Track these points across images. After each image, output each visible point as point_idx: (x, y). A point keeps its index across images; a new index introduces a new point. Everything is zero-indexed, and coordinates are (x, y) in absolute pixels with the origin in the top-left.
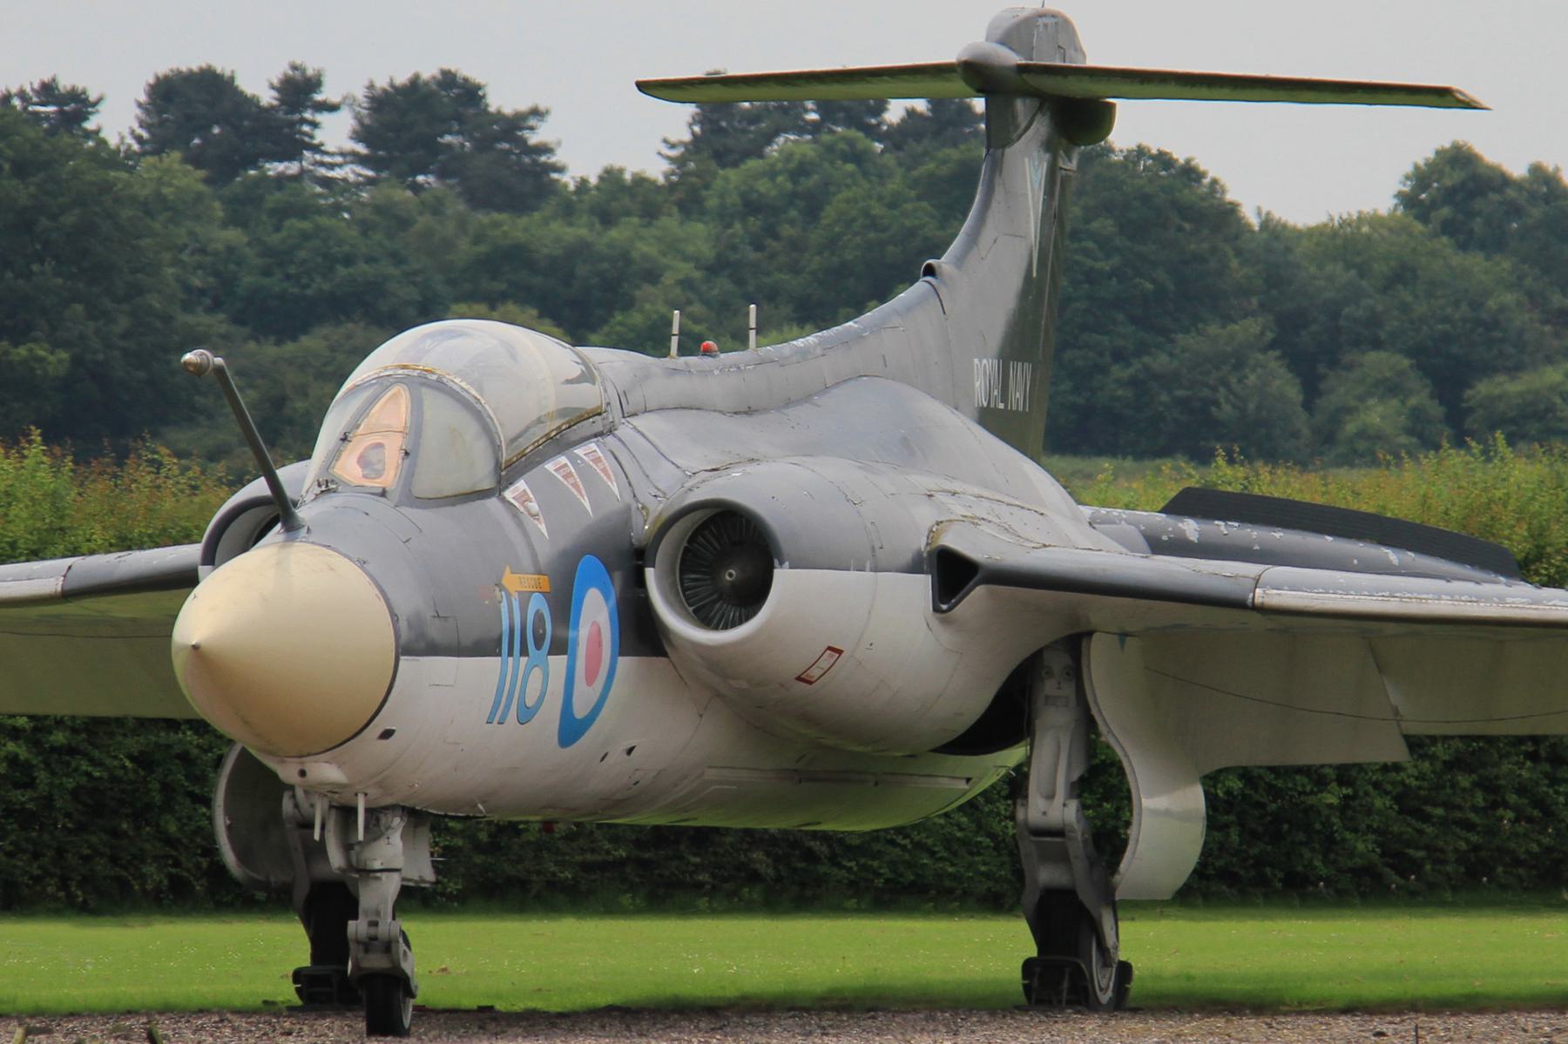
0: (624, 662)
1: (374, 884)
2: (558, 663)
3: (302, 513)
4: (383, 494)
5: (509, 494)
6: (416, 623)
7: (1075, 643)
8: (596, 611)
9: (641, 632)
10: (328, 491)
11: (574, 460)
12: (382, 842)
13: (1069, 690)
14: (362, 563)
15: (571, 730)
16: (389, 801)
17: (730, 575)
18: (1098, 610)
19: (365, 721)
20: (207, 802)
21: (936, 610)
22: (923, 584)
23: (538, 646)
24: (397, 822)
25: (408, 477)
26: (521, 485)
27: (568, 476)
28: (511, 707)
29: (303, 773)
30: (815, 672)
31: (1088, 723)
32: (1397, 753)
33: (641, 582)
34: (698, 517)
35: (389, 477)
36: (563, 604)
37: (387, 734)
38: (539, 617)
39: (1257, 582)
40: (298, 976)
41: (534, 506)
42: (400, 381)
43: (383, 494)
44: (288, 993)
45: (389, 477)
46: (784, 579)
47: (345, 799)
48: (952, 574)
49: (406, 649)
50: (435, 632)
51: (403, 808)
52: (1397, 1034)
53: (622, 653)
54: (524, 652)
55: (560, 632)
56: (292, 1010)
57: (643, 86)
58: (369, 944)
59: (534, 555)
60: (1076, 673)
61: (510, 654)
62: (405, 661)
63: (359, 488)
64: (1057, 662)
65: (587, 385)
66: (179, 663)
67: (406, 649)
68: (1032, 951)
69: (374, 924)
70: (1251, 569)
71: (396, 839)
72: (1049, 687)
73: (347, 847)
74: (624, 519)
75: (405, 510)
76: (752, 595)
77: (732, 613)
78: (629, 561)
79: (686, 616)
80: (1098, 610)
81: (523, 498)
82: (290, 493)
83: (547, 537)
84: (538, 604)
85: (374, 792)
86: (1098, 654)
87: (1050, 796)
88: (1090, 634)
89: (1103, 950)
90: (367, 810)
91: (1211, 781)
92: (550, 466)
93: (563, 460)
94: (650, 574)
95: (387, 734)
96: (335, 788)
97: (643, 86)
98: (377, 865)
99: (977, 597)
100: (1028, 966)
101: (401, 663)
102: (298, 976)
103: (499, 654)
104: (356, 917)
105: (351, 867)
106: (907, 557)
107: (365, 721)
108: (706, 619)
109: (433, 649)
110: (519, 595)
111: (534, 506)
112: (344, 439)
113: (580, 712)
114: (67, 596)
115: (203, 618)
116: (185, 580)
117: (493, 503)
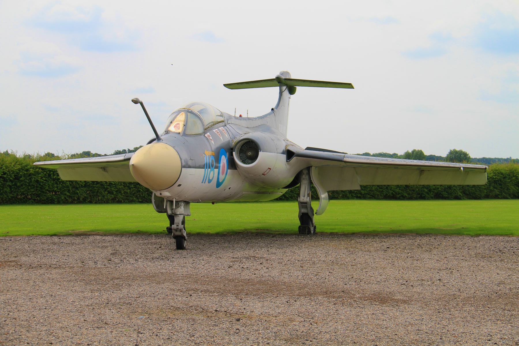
0: (229, 171)
1: (178, 217)
2: (216, 170)
5: (206, 135)
6: (186, 162)
7: (309, 168)
8: (224, 160)
9: (232, 165)
11: (219, 130)
12: (179, 208)
13: (307, 177)
14: (174, 147)
15: (219, 184)
16: (181, 200)
17: (250, 154)
18: (313, 162)
19: (175, 182)
20: (151, 196)
22: (284, 156)
23: (212, 167)
24: (182, 204)
26: (208, 134)
28: (207, 180)
29: (161, 194)
30: (266, 173)
31: (311, 183)
32: (359, 188)
33: (232, 155)
35: (180, 130)
36: (218, 159)
37: (180, 185)
39: (344, 157)
40: (167, 228)
41: (211, 138)
42: (183, 111)
43: (179, 133)
45: (180, 130)
46: (261, 154)
47: (171, 199)
48: (290, 154)
49: (183, 167)
50: (190, 163)
53: (229, 169)
54: (209, 168)
55: (217, 165)
57: (225, 85)
58: (176, 230)
59: (211, 148)
60: (309, 174)
62: (183, 169)
64: (305, 172)
66: (131, 168)
67: (183, 167)
68: (300, 225)
69: (178, 226)
71: (182, 207)
72: (304, 176)
73: (172, 209)
74: (229, 143)
75: (185, 138)
76: (254, 158)
77: (250, 161)
78: (231, 150)
80: (313, 162)
81: (209, 136)
83: (214, 144)
85: (177, 198)
87: (304, 196)
89: (312, 224)
90: (176, 202)
91: (328, 192)
94: (234, 153)
95: (180, 185)
96: (168, 197)
98: (178, 213)
99: (294, 159)
100: (299, 227)
105: (173, 213)
107: (175, 182)
108: (244, 162)
109: (190, 167)
110: (207, 157)
111: (211, 138)
112: (171, 123)
113: (220, 181)
117: (203, 136)
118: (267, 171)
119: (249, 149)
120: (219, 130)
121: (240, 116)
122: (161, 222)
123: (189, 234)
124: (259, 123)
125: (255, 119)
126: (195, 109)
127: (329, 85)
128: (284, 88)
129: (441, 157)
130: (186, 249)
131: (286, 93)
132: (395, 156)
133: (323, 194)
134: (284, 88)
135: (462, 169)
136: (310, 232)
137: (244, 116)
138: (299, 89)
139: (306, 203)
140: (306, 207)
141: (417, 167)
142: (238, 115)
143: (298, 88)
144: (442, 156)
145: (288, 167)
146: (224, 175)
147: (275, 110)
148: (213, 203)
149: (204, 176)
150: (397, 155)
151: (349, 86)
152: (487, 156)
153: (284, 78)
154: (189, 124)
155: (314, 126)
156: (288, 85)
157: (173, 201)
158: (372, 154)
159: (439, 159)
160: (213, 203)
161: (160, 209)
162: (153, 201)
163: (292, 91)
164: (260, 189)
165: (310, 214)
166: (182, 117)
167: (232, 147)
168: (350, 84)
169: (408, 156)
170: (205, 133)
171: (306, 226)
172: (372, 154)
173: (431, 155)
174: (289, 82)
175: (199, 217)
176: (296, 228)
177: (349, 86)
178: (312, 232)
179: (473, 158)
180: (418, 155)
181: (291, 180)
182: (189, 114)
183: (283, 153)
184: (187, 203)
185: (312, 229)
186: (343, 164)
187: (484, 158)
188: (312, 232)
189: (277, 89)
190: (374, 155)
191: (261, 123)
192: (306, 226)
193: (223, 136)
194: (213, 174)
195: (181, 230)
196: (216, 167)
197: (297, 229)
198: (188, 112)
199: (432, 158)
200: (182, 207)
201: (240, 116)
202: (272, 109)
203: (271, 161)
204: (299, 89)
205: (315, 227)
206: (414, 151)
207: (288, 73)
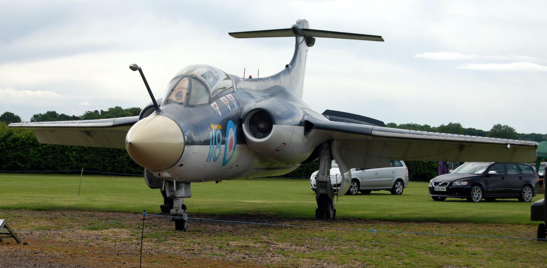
0: (237, 146)
3: (161, 108)
4: (182, 104)
6: (190, 137)
7: (329, 142)
8: (232, 134)
9: (241, 138)
10: (168, 103)
11: (226, 97)
12: (180, 190)
17: (262, 126)
18: (335, 135)
21: (305, 134)
22: (302, 129)
23: (219, 143)
25: (188, 100)
26: (215, 103)
27: (225, 101)
29: (159, 175)
33: (241, 127)
34: (254, 112)
36: (224, 131)
37: (181, 165)
38: (219, 134)
40: (161, 206)
41: (218, 108)
43: (182, 104)
44: (159, 210)
45: (183, 100)
47: (171, 180)
51: (185, 182)
52: (404, 233)
54: (215, 144)
55: (224, 139)
56: (160, 214)
57: (230, 34)
60: (330, 148)
61: (215, 144)
62: (150, 102)
63: (175, 102)
64: (325, 146)
65: (229, 80)
69: (177, 210)
70: (370, 126)
72: (323, 151)
75: (187, 108)
76: (267, 131)
77: (261, 135)
78: (239, 121)
79: (250, 135)
80: (465, 144)
81: (215, 106)
82: (158, 103)
84: (219, 132)
85: (178, 179)
86: (335, 145)
87: (324, 174)
88: (333, 140)
89: (332, 207)
90: (177, 183)
92: (221, 99)
93: (224, 97)
94: (243, 125)
95: (181, 165)
96: (168, 178)
97: (230, 34)
98: (178, 196)
99: (313, 132)
100: (317, 210)
101: (186, 147)
102: (161, 206)
103: (209, 144)
104: (172, 209)
106: (298, 123)
108: (255, 135)
113: (227, 158)
114: (114, 126)
115: (132, 136)
116: (132, 124)
117: (208, 107)
118: (282, 147)
119: (262, 120)
120: (226, 97)
121: (250, 77)
122: (155, 199)
123: (190, 215)
124: (272, 84)
125: (267, 79)
126: (198, 73)
127: (355, 37)
128: (301, 39)
129: (481, 131)
130: (185, 231)
131: (303, 45)
132: (427, 128)
133: (346, 172)
134: (301, 39)
135: (509, 146)
136: (330, 216)
137: (254, 77)
138: (318, 40)
139: (325, 182)
140: (326, 188)
141: (456, 143)
142: (247, 77)
143: (318, 40)
144: (484, 130)
145: (306, 140)
146: (232, 151)
147: (290, 66)
148: (217, 182)
149: (209, 154)
150: (429, 126)
151: (379, 38)
152: (537, 132)
153: (301, 28)
154: (193, 92)
155: (327, 86)
156: (305, 35)
157: (173, 182)
158: (398, 125)
159: (480, 133)
160: (217, 182)
161: (154, 183)
162: (145, 174)
163: (310, 42)
164: (271, 163)
165: (330, 196)
166: (185, 83)
167: (242, 117)
168: (380, 37)
169: (443, 129)
170: (210, 102)
171: (325, 210)
172: (398, 125)
173: (470, 129)
174: (308, 33)
175: (201, 197)
176: (314, 213)
177: (379, 38)
178: (331, 216)
179: (521, 133)
180: (455, 128)
181: (308, 155)
182: (193, 81)
183: (301, 124)
184: (188, 183)
185: (332, 213)
186: (370, 138)
187: (533, 134)
188: (331, 216)
189: (293, 39)
190: (402, 127)
191: (278, 87)
192: (325, 210)
193: (228, 103)
194: (219, 150)
195: (181, 215)
196: (224, 142)
197: (314, 213)
198: (193, 78)
199: (471, 132)
200: (183, 189)
201: (250, 77)
202: (287, 66)
203: (287, 132)
204: (318, 40)
205: (335, 211)
206: (450, 124)
207: (305, 22)
